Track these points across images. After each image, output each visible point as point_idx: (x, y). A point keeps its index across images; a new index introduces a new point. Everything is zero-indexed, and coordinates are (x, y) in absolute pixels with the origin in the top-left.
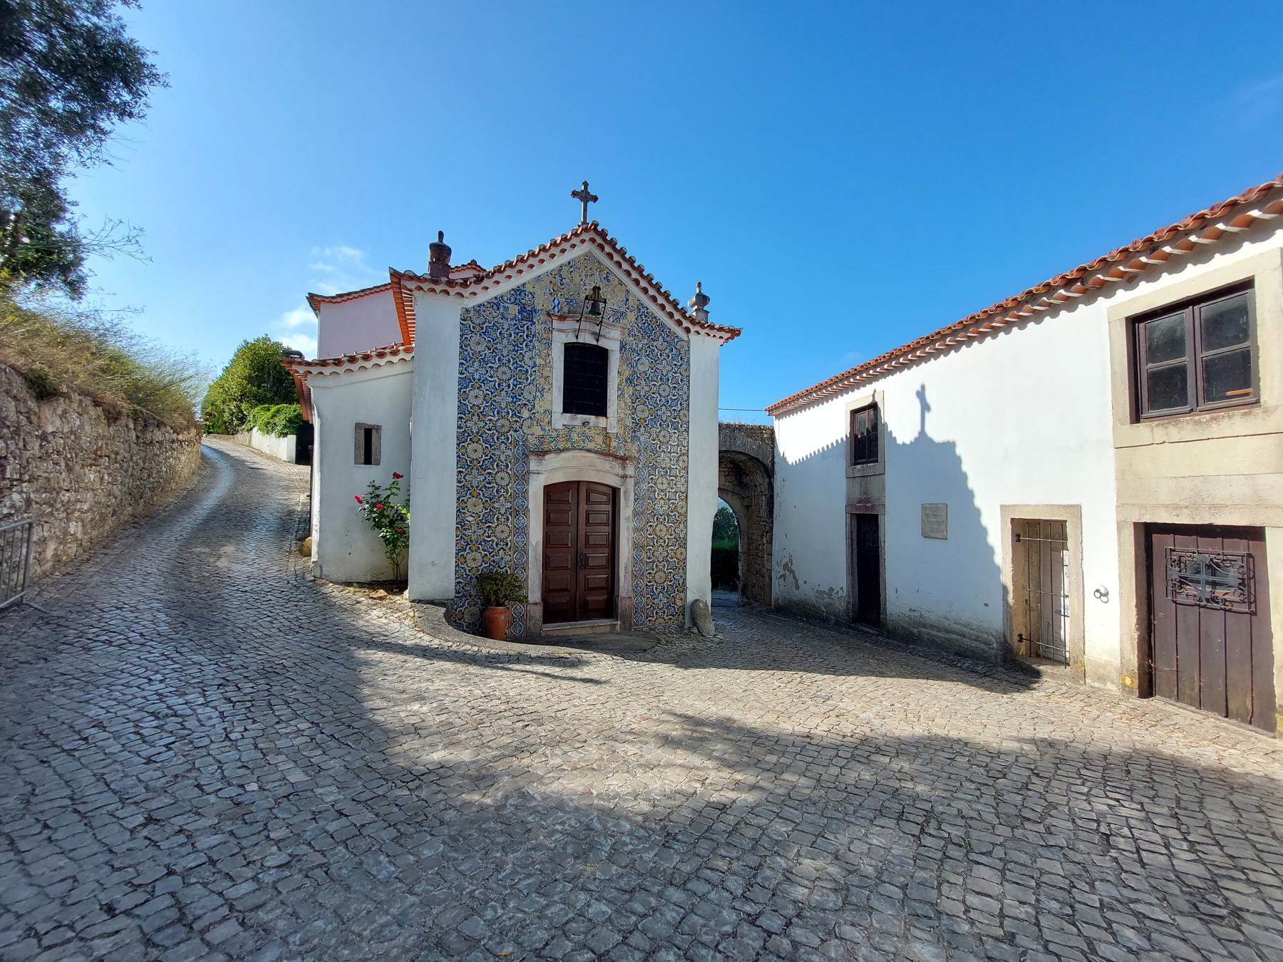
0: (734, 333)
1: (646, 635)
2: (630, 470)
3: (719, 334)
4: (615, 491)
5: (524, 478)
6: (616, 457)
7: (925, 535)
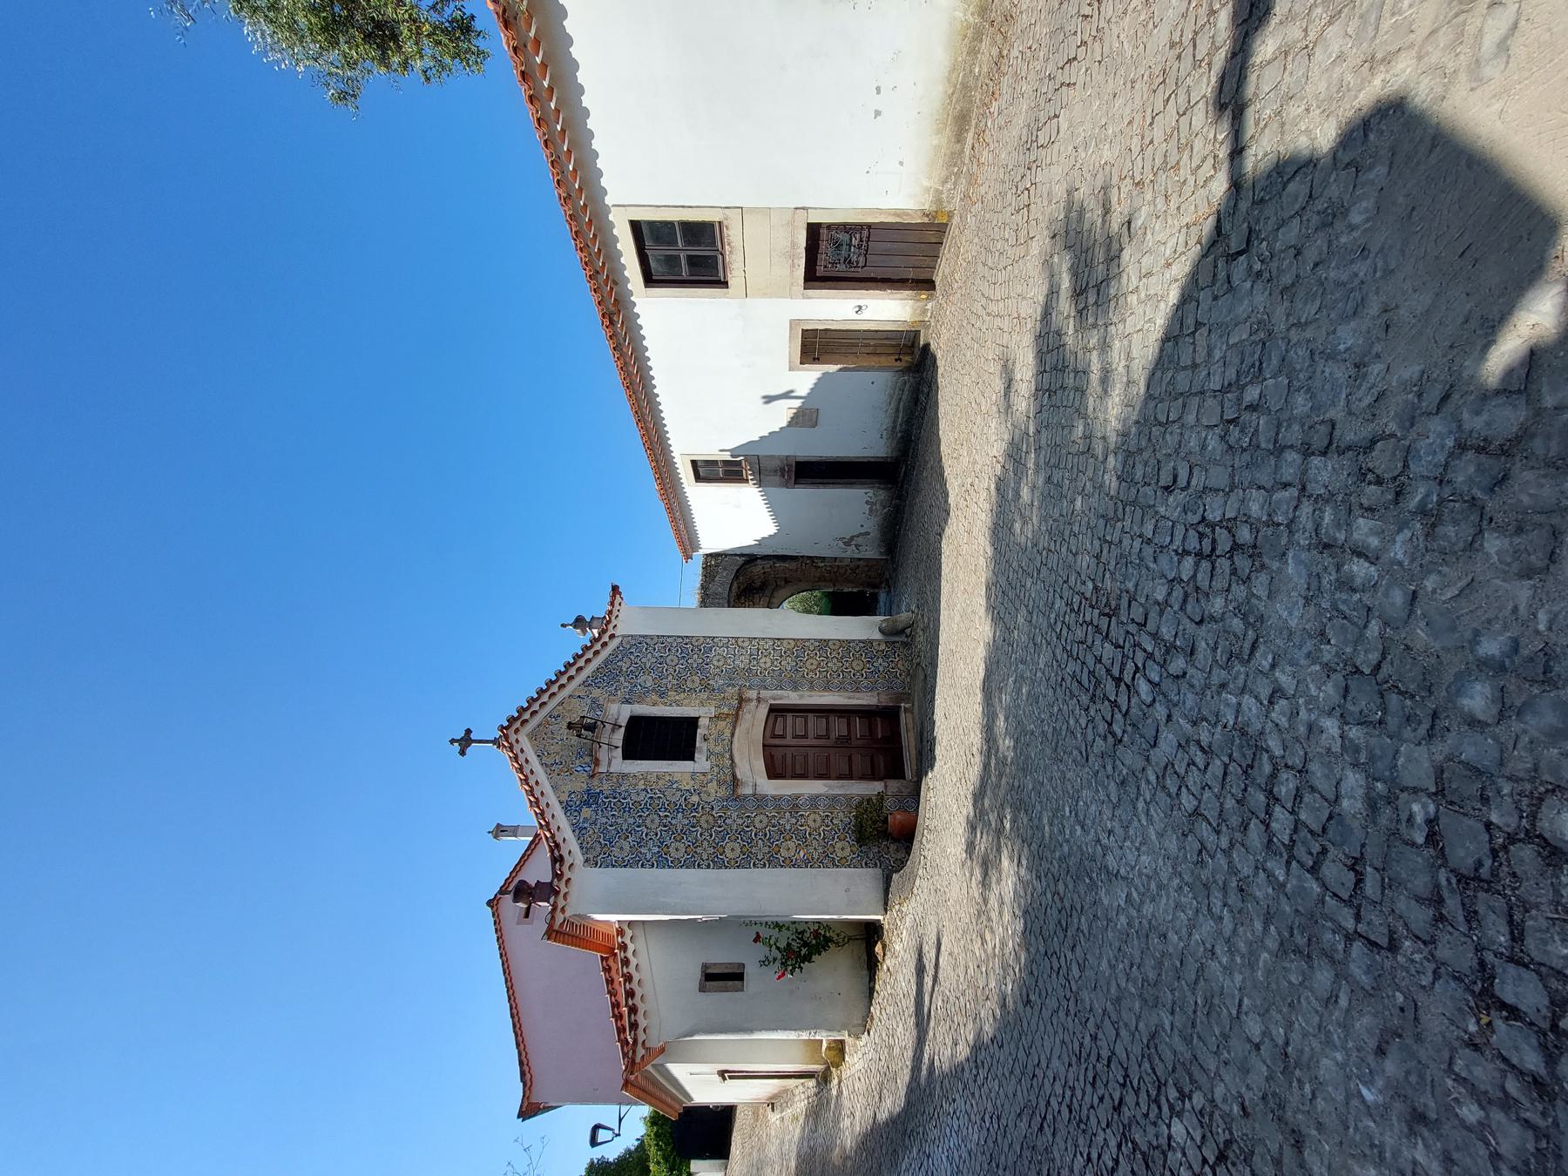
0: (615, 589)
1: (913, 677)
2: (753, 694)
3: (617, 607)
4: (776, 711)
5: (760, 800)
6: (739, 708)
7: (815, 425)
